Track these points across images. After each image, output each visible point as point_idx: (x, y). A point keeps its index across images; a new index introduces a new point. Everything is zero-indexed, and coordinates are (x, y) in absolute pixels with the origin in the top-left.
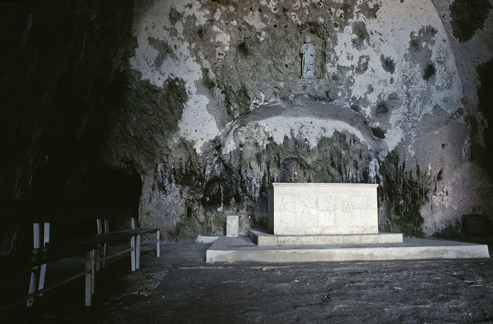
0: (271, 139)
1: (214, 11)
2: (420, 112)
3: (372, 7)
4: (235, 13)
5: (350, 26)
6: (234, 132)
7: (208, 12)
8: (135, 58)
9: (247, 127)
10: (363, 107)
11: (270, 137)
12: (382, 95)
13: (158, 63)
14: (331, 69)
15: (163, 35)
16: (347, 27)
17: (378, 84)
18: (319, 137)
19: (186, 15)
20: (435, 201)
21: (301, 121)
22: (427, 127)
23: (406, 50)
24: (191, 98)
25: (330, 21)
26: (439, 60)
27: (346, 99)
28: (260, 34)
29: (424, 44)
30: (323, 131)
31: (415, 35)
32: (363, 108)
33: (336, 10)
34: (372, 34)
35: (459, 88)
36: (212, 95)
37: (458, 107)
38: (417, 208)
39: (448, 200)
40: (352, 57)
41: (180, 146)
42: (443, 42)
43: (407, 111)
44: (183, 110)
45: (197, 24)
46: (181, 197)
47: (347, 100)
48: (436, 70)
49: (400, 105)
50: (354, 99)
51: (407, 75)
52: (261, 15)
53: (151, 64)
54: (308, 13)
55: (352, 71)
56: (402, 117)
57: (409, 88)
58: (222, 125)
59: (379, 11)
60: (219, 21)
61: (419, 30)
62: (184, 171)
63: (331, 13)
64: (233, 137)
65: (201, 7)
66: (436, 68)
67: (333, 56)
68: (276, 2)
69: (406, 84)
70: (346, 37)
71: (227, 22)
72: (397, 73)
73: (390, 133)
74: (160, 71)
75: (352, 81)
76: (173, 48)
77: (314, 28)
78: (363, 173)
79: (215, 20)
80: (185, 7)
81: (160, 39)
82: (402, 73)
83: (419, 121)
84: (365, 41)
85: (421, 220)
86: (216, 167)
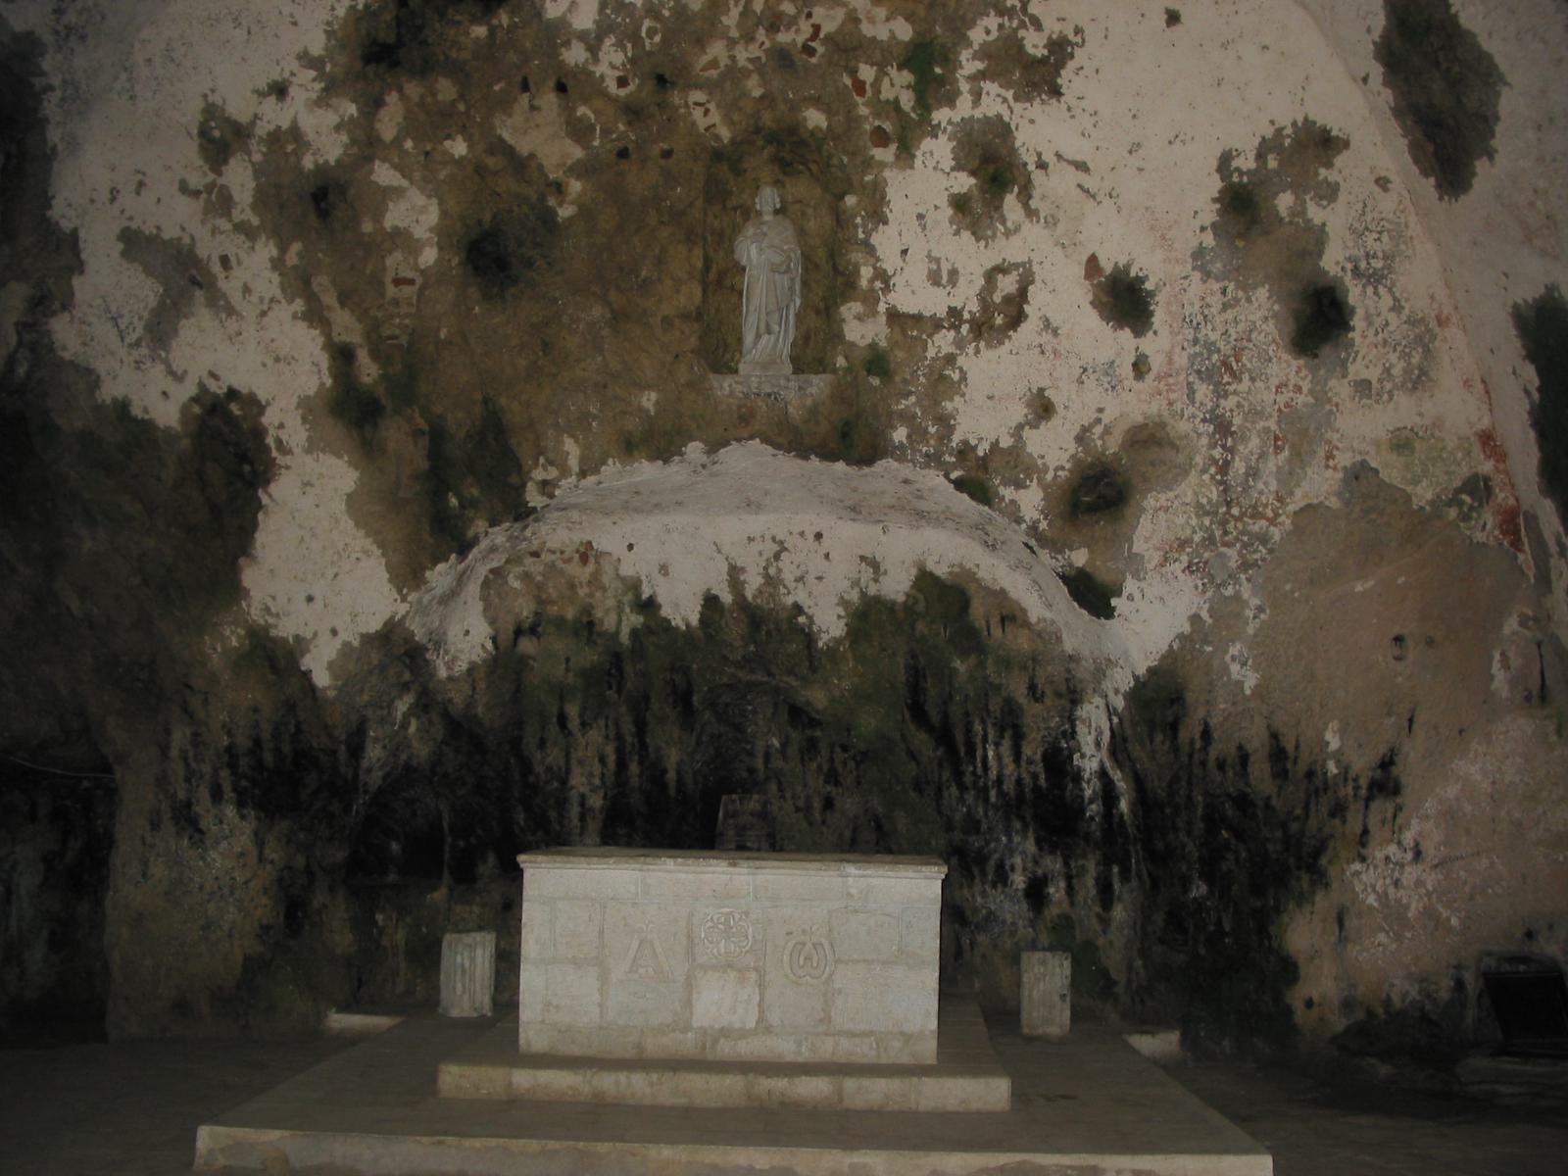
0: (649, 606)
1: (373, 105)
2: (1280, 499)
3: (1040, 52)
4: (462, 107)
5: (943, 138)
6: (486, 584)
7: (352, 109)
8: (72, 317)
10: (1006, 483)
11: (645, 596)
12: (1098, 430)
13: (160, 331)
14: (861, 330)
15: (175, 216)
16: (927, 144)
17: (1075, 387)
18: (854, 596)
19: (262, 129)
23: (1203, 229)
24: (288, 468)
25: (853, 121)
26: (1363, 265)
27: (927, 455)
28: (559, 188)
29: (1285, 202)
30: (867, 573)
33: (882, 73)
34: (1042, 165)
35: (1467, 383)
36: (368, 451)
37: (1464, 471)
38: (1264, 924)
39: (1419, 883)
40: (954, 274)
42: (1377, 189)
43: (1214, 496)
44: (260, 516)
45: (308, 163)
46: (261, 858)
48: (1353, 311)
49: (1184, 471)
50: (965, 451)
51: (1213, 336)
52: (568, 110)
53: (133, 337)
54: (757, 93)
55: (952, 333)
56: (1194, 522)
57: (1226, 396)
58: (408, 575)
59: (1071, 65)
60: (398, 141)
61: (1257, 142)
62: (268, 758)
63: (859, 87)
64: (479, 606)
65: (324, 90)
66: (1351, 300)
67: (866, 272)
70: (924, 184)
71: (428, 147)
72: (1164, 332)
73: (1137, 595)
75: (956, 376)
76: (216, 268)
77: (792, 151)
78: (1045, 757)
80: (262, 94)
81: (166, 235)
82: (1190, 334)
83: (1277, 537)
84: (1010, 201)
85: (1289, 970)
86: (412, 729)
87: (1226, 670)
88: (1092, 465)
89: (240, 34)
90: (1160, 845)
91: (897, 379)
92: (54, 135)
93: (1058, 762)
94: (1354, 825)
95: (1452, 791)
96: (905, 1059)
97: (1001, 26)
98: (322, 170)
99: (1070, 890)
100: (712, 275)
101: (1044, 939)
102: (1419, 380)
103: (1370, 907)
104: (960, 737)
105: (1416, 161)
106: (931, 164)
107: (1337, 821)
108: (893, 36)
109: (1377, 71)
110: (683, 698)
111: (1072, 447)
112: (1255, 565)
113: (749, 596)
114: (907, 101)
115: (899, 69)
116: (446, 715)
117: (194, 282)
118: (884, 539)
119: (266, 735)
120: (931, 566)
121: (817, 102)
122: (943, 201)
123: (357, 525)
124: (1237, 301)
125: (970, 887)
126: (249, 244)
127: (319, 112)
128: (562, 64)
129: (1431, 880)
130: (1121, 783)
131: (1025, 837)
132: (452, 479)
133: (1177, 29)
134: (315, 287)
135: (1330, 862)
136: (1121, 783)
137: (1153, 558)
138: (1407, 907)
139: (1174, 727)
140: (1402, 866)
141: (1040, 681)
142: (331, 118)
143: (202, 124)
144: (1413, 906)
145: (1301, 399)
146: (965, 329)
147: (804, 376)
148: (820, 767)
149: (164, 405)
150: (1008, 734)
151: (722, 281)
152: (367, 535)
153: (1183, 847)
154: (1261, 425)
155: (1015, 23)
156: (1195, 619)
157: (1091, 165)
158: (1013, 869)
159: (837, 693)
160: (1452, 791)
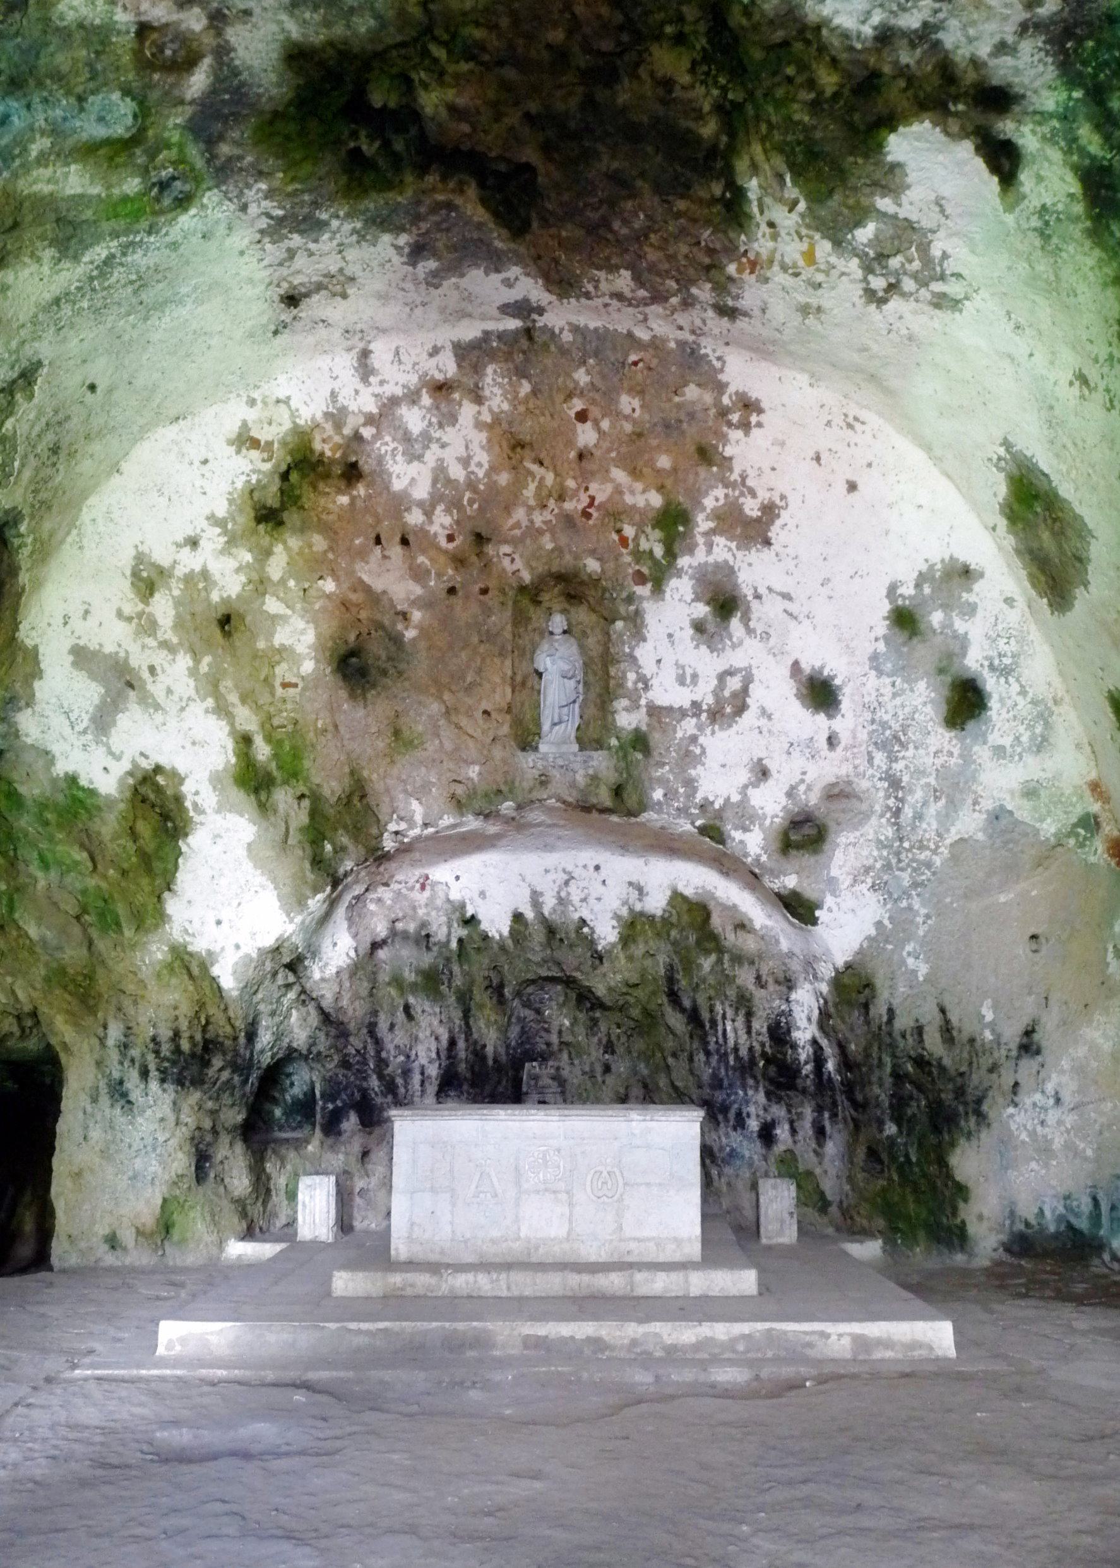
0: (471, 922)
2: (939, 835)
3: (756, 513)
5: (685, 578)
6: (351, 907)
7: (248, 557)
9: (395, 886)
10: (736, 829)
12: (802, 788)
13: (102, 722)
14: (627, 720)
15: (112, 636)
16: (674, 583)
17: (785, 756)
18: (624, 912)
19: (180, 571)
20: (1013, 1127)
21: (563, 865)
22: (968, 882)
23: (876, 640)
24: (202, 824)
26: (996, 662)
27: (678, 809)
28: (405, 616)
29: (937, 618)
31: (901, 590)
32: (737, 835)
34: (758, 597)
36: (264, 808)
37: (1078, 811)
39: (1060, 1122)
40: (695, 676)
41: (170, 967)
42: (1005, 606)
44: (180, 861)
45: (215, 597)
47: (683, 811)
49: (867, 816)
50: (704, 806)
51: (886, 717)
53: (80, 727)
54: (550, 546)
55: (694, 720)
56: (875, 853)
57: (896, 760)
59: (778, 523)
60: (283, 581)
62: (185, 1046)
63: (624, 541)
64: (345, 924)
67: (631, 676)
68: (451, 515)
69: (883, 746)
70: (673, 610)
72: (849, 715)
73: (835, 908)
74: (109, 748)
75: (698, 751)
76: (146, 675)
77: (571, 587)
78: (769, 1028)
79: (269, 579)
84: (735, 623)
86: (293, 1019)
87: (903, 962)
88: (798, 813)
89: (163, 501)
90: (859, 1097)
91: (655, 753)
92: (24, 578)
93: (780, 1033)
94: (1007, 1080)
95: (1081, 1051)
96: (678, 1257)
97: (726, 496)
98: (226, 601)
99: (794, 1131)
100: (519, 678)
101: (773, 1170)
102: (1041, 745)
103: (1023, 1142)
104: (705, 1015)
105: (1034, 586)
106: (677, 597)
107: (994, 1075)
108: (648, 504)
109: (1002, 523)
110: (497, 990)
111: (784, 801)
112: (922, 884)
113: (546, 914)
114: (659, 551)
115: (653, 528)
116: (320, 1009)
117: (130, 685)
118: (646, 869)
119: (184, 1025)
120: (681, 888)
121: (593, 553)
122: (687, 623)
123: (255, 867)
124: (903, 691)
125: (716, 1130)
126: (170, 657)
127: (222, 558)
128: (405, 524)
129: (1070, 1119)
130: (829, 1050)
131: (757, 1090)
132: (336, 840)
133: (855, 495)
134: (222, 689)
135: (990, 1107)
136: (829, 1050)
137: (845, 881)
138: (1051, 1141)
139: (866, 1006)
140: (1046, 1110)
141: (764, 972)
142: (232, 564)
143: (133, 568)
144: (1057, 1140)
145: (953, 761)
146: (704, 716)
147: (588, 753)
148: (600, 1040)
149: (105, 776)
150: (742, 1012)
151: (528, 683)
152: (263, 874)
153: (878, 1097)
154: (923, 781)
155: (737, 493)
156: (879, 924)
157: (793, 595)
158: (748, 1115)
159: (612, 984)
160: (1081, 1051)
